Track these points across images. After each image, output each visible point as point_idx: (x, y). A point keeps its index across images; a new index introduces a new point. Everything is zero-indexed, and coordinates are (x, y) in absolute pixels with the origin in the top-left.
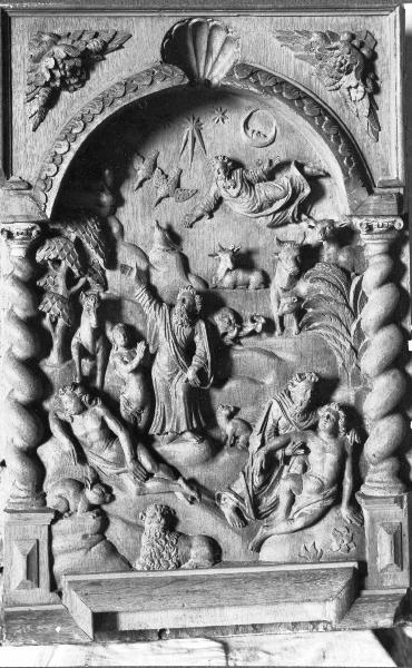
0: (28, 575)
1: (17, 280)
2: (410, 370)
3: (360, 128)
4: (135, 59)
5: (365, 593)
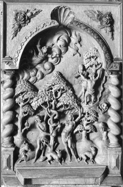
4: (42, 20)
5: (109, 175)
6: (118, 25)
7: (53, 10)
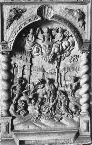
0: (7, 131)
1: (3, 80)
2: (91, 103)
3: (80, 30)
4: (31, 12)
5: (79, 136)
6: (88, 20)
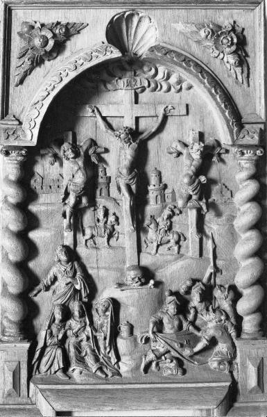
4: (89, 47)
7: (111, 22)
